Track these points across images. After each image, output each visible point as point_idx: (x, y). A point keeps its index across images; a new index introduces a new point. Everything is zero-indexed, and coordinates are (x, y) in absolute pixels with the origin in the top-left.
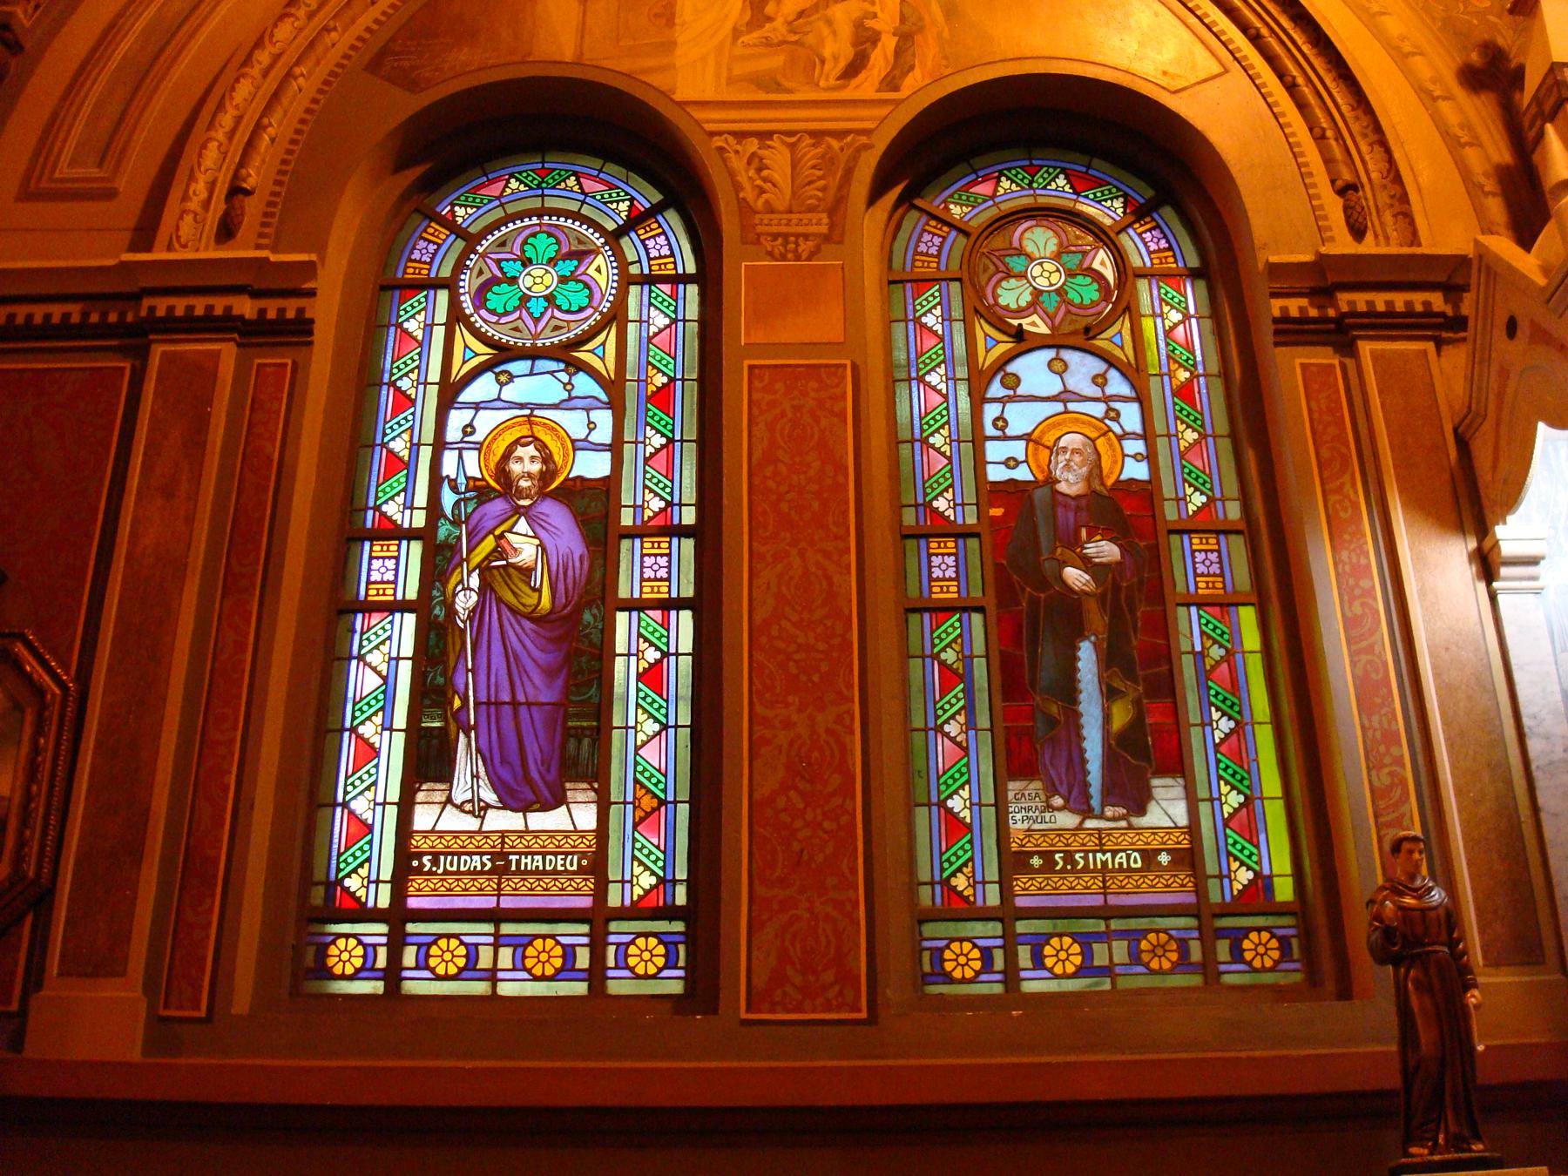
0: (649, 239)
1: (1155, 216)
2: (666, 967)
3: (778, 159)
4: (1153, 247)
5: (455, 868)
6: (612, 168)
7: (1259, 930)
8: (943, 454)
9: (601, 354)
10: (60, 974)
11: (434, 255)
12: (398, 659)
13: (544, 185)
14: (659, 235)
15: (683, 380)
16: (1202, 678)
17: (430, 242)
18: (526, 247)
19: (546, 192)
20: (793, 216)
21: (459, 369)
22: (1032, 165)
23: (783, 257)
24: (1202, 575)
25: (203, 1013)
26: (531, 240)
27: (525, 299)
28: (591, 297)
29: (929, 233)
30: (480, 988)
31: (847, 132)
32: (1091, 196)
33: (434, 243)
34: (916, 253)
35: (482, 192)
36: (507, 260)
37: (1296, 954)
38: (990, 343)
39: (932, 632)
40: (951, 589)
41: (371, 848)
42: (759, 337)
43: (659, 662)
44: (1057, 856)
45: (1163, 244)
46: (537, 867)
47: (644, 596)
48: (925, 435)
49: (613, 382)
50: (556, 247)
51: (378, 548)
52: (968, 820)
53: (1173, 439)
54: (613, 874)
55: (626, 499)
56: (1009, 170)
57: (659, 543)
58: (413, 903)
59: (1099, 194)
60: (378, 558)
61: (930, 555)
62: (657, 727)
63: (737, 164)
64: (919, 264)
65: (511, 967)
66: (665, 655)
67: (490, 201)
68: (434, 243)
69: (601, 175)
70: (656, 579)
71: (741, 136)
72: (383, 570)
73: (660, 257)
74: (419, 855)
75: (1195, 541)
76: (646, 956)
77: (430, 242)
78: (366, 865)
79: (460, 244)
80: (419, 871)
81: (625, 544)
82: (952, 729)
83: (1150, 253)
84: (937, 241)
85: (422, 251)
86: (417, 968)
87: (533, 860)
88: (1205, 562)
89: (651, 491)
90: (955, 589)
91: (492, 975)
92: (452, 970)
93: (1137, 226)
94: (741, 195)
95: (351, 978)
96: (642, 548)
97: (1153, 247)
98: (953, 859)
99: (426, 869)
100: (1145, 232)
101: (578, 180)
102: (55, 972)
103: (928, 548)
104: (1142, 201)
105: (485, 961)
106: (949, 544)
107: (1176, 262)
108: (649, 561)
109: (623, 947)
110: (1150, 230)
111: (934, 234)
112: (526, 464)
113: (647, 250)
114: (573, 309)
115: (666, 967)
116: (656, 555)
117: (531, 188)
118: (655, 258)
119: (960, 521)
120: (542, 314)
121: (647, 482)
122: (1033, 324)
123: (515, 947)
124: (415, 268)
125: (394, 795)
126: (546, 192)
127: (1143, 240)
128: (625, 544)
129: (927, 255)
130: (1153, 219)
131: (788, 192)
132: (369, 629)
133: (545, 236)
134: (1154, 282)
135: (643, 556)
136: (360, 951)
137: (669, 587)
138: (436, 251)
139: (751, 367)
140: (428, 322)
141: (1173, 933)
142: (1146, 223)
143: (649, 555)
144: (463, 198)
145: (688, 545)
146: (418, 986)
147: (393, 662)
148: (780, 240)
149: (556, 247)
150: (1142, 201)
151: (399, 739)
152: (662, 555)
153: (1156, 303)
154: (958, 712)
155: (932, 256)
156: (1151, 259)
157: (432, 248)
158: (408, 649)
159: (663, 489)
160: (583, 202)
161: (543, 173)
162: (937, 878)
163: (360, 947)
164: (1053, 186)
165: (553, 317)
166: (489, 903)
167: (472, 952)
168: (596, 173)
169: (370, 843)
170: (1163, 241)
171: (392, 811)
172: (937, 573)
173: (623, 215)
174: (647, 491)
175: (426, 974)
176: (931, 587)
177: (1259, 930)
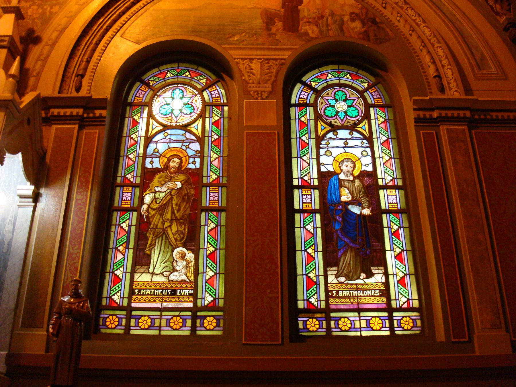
0: (212, 91)
1: (364, 88)
2: (216, 326)
3: (255, 66)
4: (375, 97)
5: (360, 295)
6: (200, 68)
7: (210, 316)
8: (307, 162)
9: (364, 129)
10: (22, 327)
11: (144, 95)
12: (123, 298)
13: (179, 75)
14: (215, 90)
15: (223, 137)
16: (390, 235)
17: (143, 91)
18: (335, 95)
19: (341, 79)
20: (261, 85)
21: (321, 133)
22: (339, 71)
23: (257, 99)
24: (305, 203)
25: (280, 343)
26: (337, 93)
27: (337, 112)
28: (358, 112)
29: (304, 91)
30: (156, 332)
31: (277, 59)
32: (196, 79)
33: (144, 91)
34: (136, 96)
35: (158, 76)
36: (331, 99)
37: (222, 325)
38: (364, 128)
39: (120, 217)
40: (216, 204)
41: (121, 287)
42: (250, 124)
43: (214, 252)
44: (136, 291)
45: (378, 96)
46: (148, 293)
47: (210, 206)
48: (128, 154)
49: (319, 137)
50: (345, 96)
51: (125, 189)
52: (315, 281)
53: (310, 157)
54: (199, 296)
55: (379, 176)
56: (171, 70)
57: (215, 189)
58: (133, 305)
59: (198, 78)
60: (125, 192)
61: (123, 193)
62: (213, 274)
63: (242, 67)
64: (136, 100)
65: (134, 325)
66: (216, 249)
67: (323, 81)
68: (144, 91)
69: (197, 71)
70: (214, 200)
71: (243, 59)
72: (214, 196)
73: (216, 97)
74: (332, 291)
75: (211, 189)
76: (210, 323)
77: (143, 91)
78: (120, 292)
79: (152, 92)
80: (332, 296)
81: (204, 189)
82: (121, 248)
83: (374, 99)
84: (306, 94)
85: (141, 94)
86: (135, 326)
87: (146, 291)
88: (127, 196)
89: (213, 172)
90: (217, 204)
91: (160, 328)
92: (147, 327)
93: (370, 90)
94: (243, 78)
95: (348, 331)
96: (210, 190)
97: (375, 97)
98: (114, 290)
99: (334, 295)
100: (373, 92)
101: (189, 73)
102: (20, 325)
103: (123, 190)
104: (372, 83)
105: (157, 324)
106: (309, 192)
107: (382, 102)
108: (212, 194)
109: (368, 321)
110: (374, 92)
111: (306, 92)
112: (174, 163)
113: (308, 96)
114: (188, 113)
115: (216, 326)
116: (214, 193)
117: (175, 76)
118: (214, 98)
119: (134, 182)
120: (344, 118)
121: (211, 169)
122: (336, 122)
123: (136, 319)
124: (137, 99)
125: (129, 270)
126: (341, 79)
127: (372, 95)
128: (204, 189)
129: (303, 98)
130: (375, 88)
131: (259, 76)
132: (119, 239)
133: (341, 92)
134: (375, 108)
135: (210, 193)
136: (117, 320)
137: (218, 203)
138: (308, 95)
139: (247, 133)
140: (211, 118)
141: (151, 317)
142: (373, 90)
143: (212, 193)
144: (152, 78)
145: (317, 192)
146: (134, 332)
147: (315, 229)
148: (256, 93)
149: (345, 96)
150: (372, 83)
151: (320, 254)
152: (309, 195)
153: (376, 115)
154: (124, 243)
155: (305, 99)
156: (374, 101)
157: (143, 93)
158: (134, 222)
159: (217, 172)
160: (353, 82)
161: (339, 72)
162: (300, 177)
163: (117, 319)
164: (346, 77)
165: (347, 119)
166: (159, 306)
167: (153, 321)
168: (195, 70)
169: (121, 285)
170: (378, 95)
171: (128, 275)
172: (124, 198)
173: (204, 84)
174: (211, 172)
175: (203, 329)
176: (122, 203)
177: (210, 316)
